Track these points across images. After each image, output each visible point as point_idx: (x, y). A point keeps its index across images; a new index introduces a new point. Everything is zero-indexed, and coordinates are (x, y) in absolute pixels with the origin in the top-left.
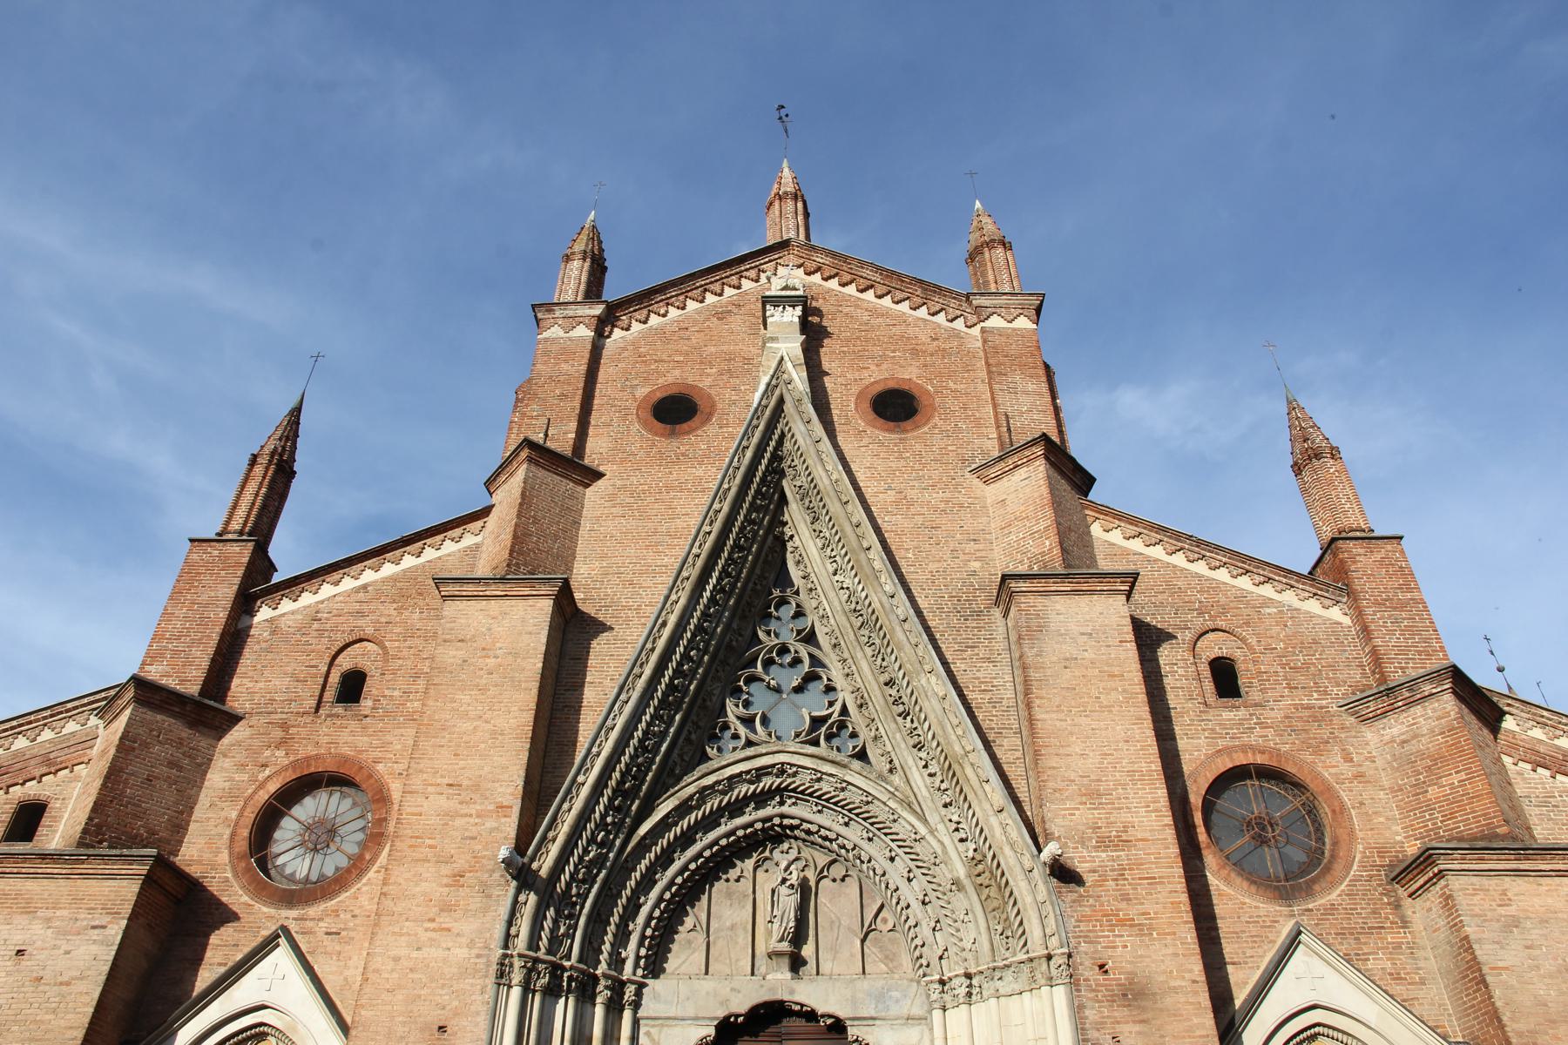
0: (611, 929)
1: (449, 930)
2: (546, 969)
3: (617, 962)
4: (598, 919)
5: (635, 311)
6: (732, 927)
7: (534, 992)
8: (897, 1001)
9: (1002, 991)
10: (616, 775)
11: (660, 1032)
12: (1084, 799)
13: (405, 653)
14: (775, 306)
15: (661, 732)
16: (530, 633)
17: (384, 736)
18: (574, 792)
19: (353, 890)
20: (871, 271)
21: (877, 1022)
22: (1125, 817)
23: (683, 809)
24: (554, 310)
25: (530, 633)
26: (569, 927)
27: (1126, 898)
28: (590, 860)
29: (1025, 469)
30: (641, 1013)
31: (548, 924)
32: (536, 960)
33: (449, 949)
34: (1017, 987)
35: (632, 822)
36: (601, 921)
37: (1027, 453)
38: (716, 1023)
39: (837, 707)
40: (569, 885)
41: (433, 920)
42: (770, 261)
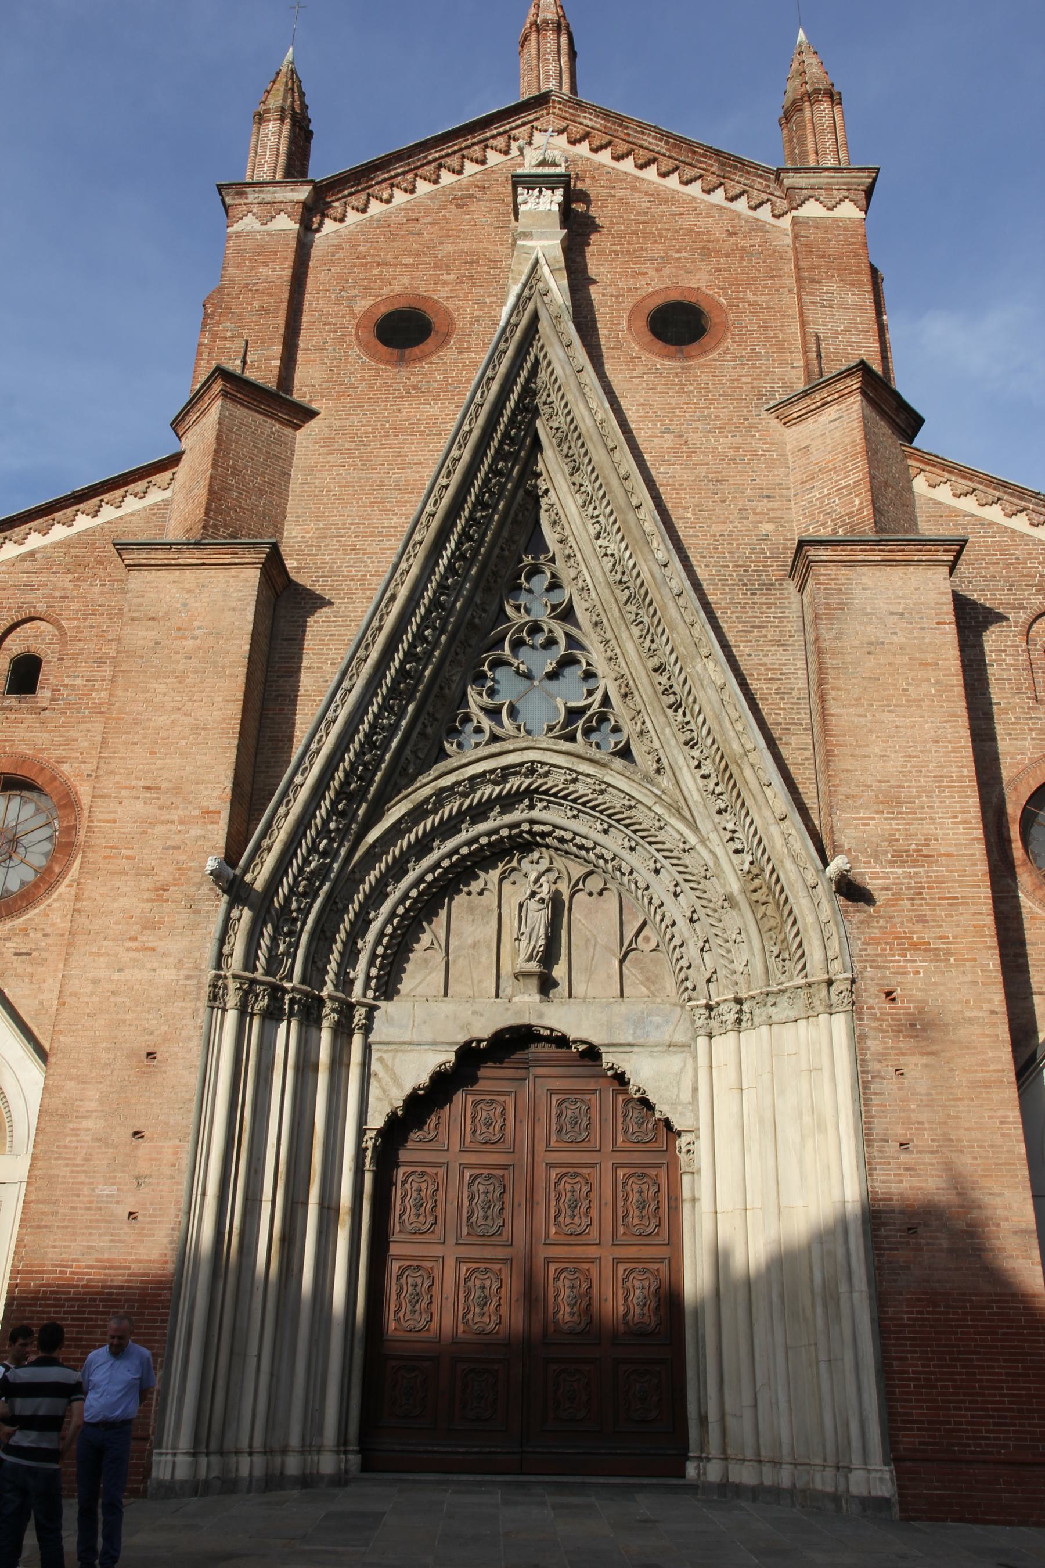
0: (338, 947)
1: (153, 949)
2: (264, 990)
3: (345, 983)
4: (322, 936)
5: (351, 194)
6: (475, 945)
7: (252, 1015)
8: (658, 1027)
9: (775, 1018)
10: (340, 775)
11: (394, 1058)
12: (881, 808)
13: (86, 634)
14: (528, 189)
15: (390, 725)
16: (234, 610)
17: (68, 731)
18: (291, 795)
19: (42, 907)
20: (655, 138)
21: (635, 1049)
22: (929, 828)
23: (418, 813)
24: (245, 193)
25: (234, 610)
26: (289, 945)
27: (922, 920)
28: (312, 872)
29: (836, 407)
30: (372, 1038)
31: (265, 942)
32: (253, 982)
33: (155, 970)
34: (792, 1014)
35: (358, 828)
36: (326, 939)
37: (839, 386)
38: (456, 1048)
39: (598, 696)
40: (287, 899)
41: (134, 939)
42: (524, 124)
